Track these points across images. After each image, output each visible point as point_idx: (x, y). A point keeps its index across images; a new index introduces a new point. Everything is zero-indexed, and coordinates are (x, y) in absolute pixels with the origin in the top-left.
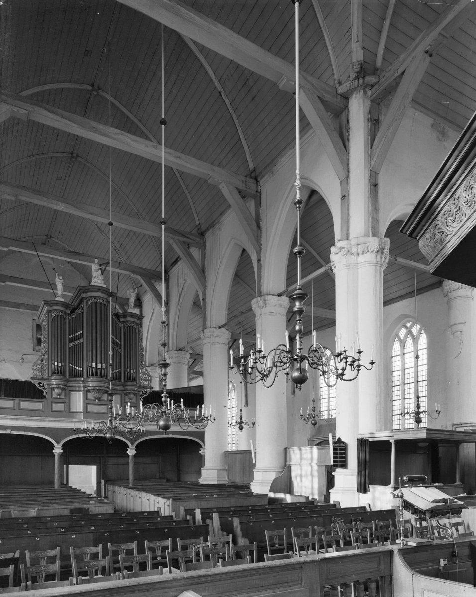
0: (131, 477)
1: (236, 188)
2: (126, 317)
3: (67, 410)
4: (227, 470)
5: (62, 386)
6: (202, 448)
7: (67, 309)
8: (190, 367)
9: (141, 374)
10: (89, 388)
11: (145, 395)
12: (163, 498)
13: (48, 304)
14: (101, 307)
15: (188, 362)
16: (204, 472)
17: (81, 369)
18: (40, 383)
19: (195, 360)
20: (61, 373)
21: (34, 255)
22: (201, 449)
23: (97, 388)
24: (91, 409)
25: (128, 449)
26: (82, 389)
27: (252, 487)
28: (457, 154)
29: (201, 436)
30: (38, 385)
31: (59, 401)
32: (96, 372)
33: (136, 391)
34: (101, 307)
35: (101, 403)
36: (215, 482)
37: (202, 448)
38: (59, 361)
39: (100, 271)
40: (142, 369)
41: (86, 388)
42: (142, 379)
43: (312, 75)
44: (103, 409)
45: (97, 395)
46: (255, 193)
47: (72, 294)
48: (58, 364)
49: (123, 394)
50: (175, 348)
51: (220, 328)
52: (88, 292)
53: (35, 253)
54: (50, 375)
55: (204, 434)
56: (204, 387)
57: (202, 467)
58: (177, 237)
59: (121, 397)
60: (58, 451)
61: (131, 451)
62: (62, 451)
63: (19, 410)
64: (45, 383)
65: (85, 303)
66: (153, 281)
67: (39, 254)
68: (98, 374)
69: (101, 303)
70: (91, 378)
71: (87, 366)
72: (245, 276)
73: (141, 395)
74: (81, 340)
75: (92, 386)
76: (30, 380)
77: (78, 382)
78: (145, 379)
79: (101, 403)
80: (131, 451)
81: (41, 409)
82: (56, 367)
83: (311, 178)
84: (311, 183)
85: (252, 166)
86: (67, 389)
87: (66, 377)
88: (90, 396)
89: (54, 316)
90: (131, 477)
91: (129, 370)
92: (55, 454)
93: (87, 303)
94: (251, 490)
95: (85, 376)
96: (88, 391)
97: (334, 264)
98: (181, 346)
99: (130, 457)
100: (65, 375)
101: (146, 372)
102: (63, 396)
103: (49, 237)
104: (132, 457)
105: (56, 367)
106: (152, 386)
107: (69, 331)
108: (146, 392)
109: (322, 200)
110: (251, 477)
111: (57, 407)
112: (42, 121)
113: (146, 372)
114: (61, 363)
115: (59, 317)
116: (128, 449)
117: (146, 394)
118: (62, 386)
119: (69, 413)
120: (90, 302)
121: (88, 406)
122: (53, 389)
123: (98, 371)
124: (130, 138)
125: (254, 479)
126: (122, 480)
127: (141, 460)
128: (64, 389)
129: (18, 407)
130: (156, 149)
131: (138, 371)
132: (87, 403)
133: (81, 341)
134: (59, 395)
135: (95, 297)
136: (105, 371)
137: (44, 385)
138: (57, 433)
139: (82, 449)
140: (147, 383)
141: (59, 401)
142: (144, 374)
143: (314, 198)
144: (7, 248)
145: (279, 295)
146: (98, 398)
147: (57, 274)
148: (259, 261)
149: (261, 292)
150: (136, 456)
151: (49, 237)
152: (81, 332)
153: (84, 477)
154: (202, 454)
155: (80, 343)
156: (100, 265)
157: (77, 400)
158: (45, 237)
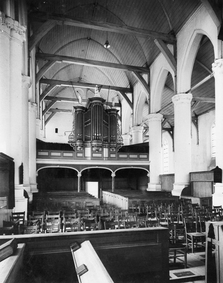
0: (113, 188)
1: (162, 40)
2: (110, 111)
3: (83, 156)
4: (161, 184)
5: (81, 145)
6: (148, 173)
7: (83, 110)
8: (144, 133)
10: (93, 145)
11: (120, 148)
12: (125, 197)
13: (75, 108)
14: (99, 108)
15: (143, 131)
16: (149, 185)
17: (90, 137)
18: (71, 144)
19: (146, 130)
21: (71, 87)
23: (97, 145)
24: (94, 155)
25: (112, 174)
26: (90, 146)
27: (172, 193)
29: (148, 167)
30: (71, 145)
31: (80, 152)
32: (96, 138)
33: (115, 146)
34: (99, 108)
35: (100, 152)
36: (155, 190)
37: (148, 173)
38: (80, 134)
39: (98, 90)
40: (118, 135)
41: (92, 146)
44: (100, 155)
45: (97, 149)
46: (173, 42)
47: (86, 103)
48: (113, 137)
49: (109, 148)
50: (136, 125)
51: (157, 113)
52: (93, 100)
53: (72, 86)
54: (76, 140)
55: (149, 167)
56: (149, 143)
57: (148, 183)
58: (135, 70)
59: (108, 149)
60: (79, 175)
61: (113, 175)
63: (77, 157)
64: (74, 144)
65: (91, 106)
66: (126, 94)
67: (73, 86)
68: (97, 139)
69: (99, 106)
70: (94, 141)
71: (92, 135)
72: (169, 84)
73: (118, 148)
74: (90, 123)
75: (95, 145)
76: (67, 143)
77: (88, 143)
79: (100, 152)
80: (113, 175)
81: (115, 157)
82: (95, 137)
83: (202, 29)
84: (203, 32)
85: (171, 28)
86: (84, 146)
87: (108, 142)
88: (94, 149)
89: (78, 113)
90: (113, 188)
91: (112, 136)
92: (78, 176)
93: (92, 106)
94: (172, 194)
95: (92, 140)
96: (93, 147)
97: (214, 73)
98: (139, 124)
99: (113, 178)
100: (83, 140)
102: (82, 150)
103: (80, 78)
104: (114, 178)
105: (95, 137)
106: (123, 143)
107: (84, 120)
108: (120, 146)
109: (209, 41)
110: (172, 188)
111: (79, 155)
112: (70, 24)
114: (81, 134)
115: (80, 113)
116: (112, 174)
117: (120, 147)
118: (81, 145)
119: (84, 158)
120: (94, 105)
121: (93, 154)
122: (77, 146)
124: (109, 24)
125: (173, 189)
126: (108, 189)
127: (119, 179)
128: (82, 147)
129: (84, 156)
130: (122, 27)
131: (116, 136)
132: (110, 153)
133: (90, 123)
134: (80, 149)
135: (96, 103)
136: (101, 137)
137: (73, 145)
138: (113, 167)
139: (93, 174)
141: (80, 152)
142: (119, 138)
143: (205, 39)
144: (60, 85)
145: (187, 93)
146: (98, 150)
148: (176, 76)
149: (177, 92)
150: (115, 177)
151: (80, 78)
152: (90, 119)
153: (92, 187)
154: (148, 176)
155: (89, 125)
156: (98, 88)
157: (88, 151)
158: (79, 79)
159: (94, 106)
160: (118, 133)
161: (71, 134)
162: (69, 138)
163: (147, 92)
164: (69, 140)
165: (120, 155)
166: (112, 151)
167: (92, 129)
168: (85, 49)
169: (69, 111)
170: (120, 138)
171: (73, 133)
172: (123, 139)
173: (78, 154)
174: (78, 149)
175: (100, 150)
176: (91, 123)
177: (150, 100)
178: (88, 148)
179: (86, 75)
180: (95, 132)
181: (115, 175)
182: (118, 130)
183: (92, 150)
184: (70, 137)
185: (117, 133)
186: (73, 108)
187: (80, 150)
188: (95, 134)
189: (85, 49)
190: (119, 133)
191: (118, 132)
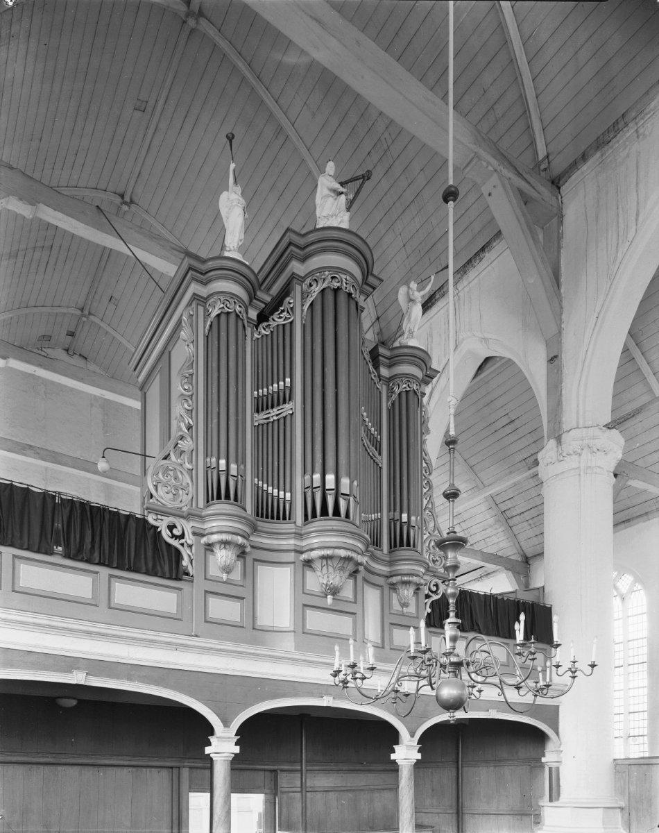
11: (435, 597)
18: (171, 527)
30: (165, 534)
64: (187, 526)
73: (427, 596)
88: (316, 581)
103: (86, 312)
119: (251, 631)
120: (316, 289)
121: (310, 613)
122: (209, 547)
133: (287, 408)
134: (228, 570)
137: (182, 536)
147: (233, 166)
151: (86, 312)
152: (288, 380)
157: (277, 589)
165: (238, 619)
166: (400, 609)
167: (404, 412)
168: (152, 102)
169: (28, 452)
173: (213, 602)
174: (214, 571)
175: (348, 593)
177: (559, 370)
179: (116, 295)
182: (425, 490)
183: (300, 586)
187: (225, 576)
189: (152, 102)
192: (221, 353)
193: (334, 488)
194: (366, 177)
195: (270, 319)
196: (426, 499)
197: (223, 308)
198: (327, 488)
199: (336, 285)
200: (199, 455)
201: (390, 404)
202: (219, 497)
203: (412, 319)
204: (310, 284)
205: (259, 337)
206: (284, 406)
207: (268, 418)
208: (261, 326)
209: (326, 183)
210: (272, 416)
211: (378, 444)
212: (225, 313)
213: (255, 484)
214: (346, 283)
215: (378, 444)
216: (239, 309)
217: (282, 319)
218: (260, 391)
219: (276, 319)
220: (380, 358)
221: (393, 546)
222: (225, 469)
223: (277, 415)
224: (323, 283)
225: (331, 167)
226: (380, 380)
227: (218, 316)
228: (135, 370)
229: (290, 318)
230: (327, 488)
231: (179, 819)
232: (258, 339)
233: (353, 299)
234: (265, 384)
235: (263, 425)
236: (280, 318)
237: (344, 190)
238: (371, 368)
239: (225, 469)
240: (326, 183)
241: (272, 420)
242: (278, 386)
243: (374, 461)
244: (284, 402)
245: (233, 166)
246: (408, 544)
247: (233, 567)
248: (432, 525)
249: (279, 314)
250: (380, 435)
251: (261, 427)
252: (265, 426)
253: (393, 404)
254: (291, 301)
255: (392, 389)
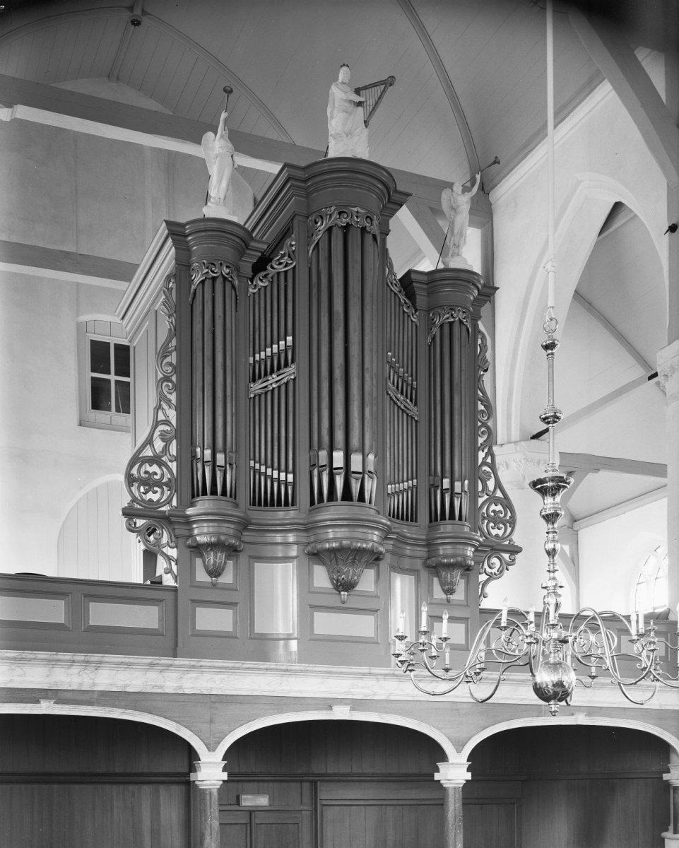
9: (481, 501)
20: (224, 493)
22: (441, 765)
28: (326, 282)
42: (484, 518)
43: (118, 79)
44: (362, 626)
62: (469, 776)
63: (310, 592)
78: (496, 520)
82: (276, 485)
101: (499, 494)
102: (227, 578)
104: (459, 796)
113: (499, 494)
119: (254, 647)
123: (353, 482)
133: (290, 372)
140: (500, 533)
142: (493, 499)
147: (224, 115)
152: (289, 339)
159: (330, 230)
160: (484, 463)
161: (148, 452)
162: (130, 480)
163: (591, 250)
164: (134, 500)
170: (496, 501)
171: (648, 657)
172: (512, 511)
176: (298, 369)
178: (279, 567)
180: (339, 436)
181: (469, 776)
182: (481, 440)
184: (134, 471)
185: (480, 461)
186: (163, 230)
188: (339, 458)
190: (489, 460)
191: (481, 455)
192: (210, 313)
193: (342, 466)
194: (389, 82)
195: (269, 268)
196: (483, 451)
197: (208, 272)
198: (334, 466)
199: (344, 221)
200: (230, 367)
201: (429, 339)
202: (204, 493)
203: (456, 231)
204: (315, 220)
205: (255, 291)
206: (286, 370)
207: (266, 387)
208: (256, 279)
209: (339, 94)
210: (271, 384)
211: (414, 392)
212: (209, 279)
213: (250, 467)
214: (357, 217)
215: (414, 392)
216: (228, 271)
217: (281, 266)
218: (257, 356)
219: (276, 266)
220: (415, 284)
221: (433, 518)
222: (291, 345)
223: (277, 382)
224: (330, 219)
225: (343, 74)
226: (416, 311)
227: (203, 282)
228: (123, 318)
229: (291, 264)
230: (334, 466)
231: (662, 842)
232: (254, 294)
233: (368, 232)
234: (263, 347)
235: (260, 395)
236: (280, 264)
237: (362, 99)
238: (403, 298)
239: (291, 345)
240: (339, 94)
241: (271, 388)
242: (279, 346)
243: (407, 415)
244: (286, 365)
245: (224, 115)
246: (452, 516)
247: (223, 569)
248: (491, 484)
249: (278, 260)
250: (416, 381)
251: (257, 397)
252: (263, 397)
253: (434, 339)
254: (293, 243)
255: (433, 320)
